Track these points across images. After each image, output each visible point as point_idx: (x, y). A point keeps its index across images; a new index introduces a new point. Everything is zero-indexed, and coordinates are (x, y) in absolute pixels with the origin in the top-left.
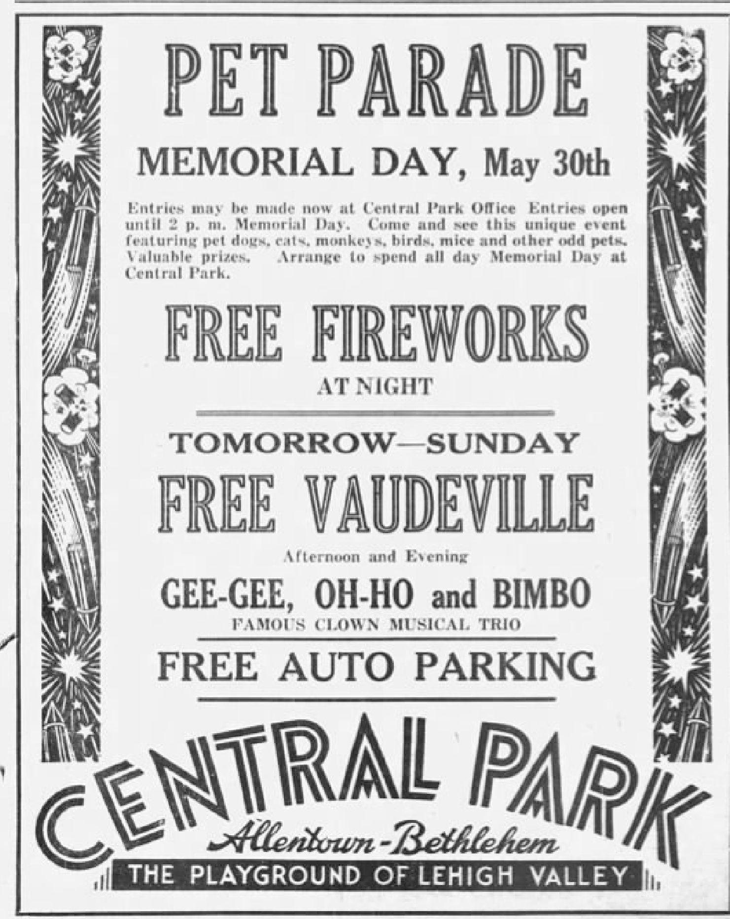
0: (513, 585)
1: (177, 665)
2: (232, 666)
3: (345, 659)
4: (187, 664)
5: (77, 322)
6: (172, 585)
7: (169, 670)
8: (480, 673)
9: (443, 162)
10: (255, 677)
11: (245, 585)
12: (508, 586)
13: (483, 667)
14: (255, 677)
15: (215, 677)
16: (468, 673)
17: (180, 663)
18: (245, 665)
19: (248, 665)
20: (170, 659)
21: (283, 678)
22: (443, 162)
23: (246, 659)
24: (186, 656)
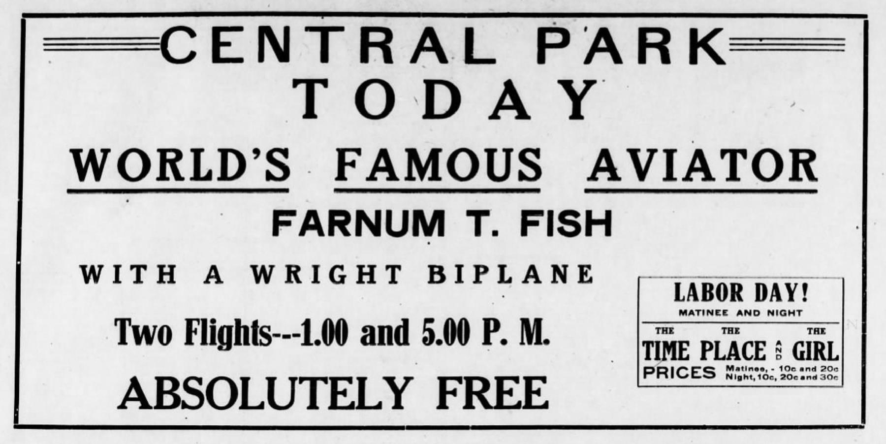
0: (827, 346)
1: (458, 392)
2: (519, 393)
3: (307, 384)
4: (469, 392)
5: (715, 304)
6: (799, 345)
7: (449, 397)
8: (476, 401)
9: (398, 393)
10: (546, 406)
11: (803, 345)
12: (823, 347)
13: (479, 394)
14: (546, 406)
15: (500, 405)
16: (152, 400)
17: (462, 389)
18: (535, 392)
19: (538, 392)
20: (450, 385)
21: (122, 406)
22: (398, 393)
23: (536, 385)
24: (469, 380)
